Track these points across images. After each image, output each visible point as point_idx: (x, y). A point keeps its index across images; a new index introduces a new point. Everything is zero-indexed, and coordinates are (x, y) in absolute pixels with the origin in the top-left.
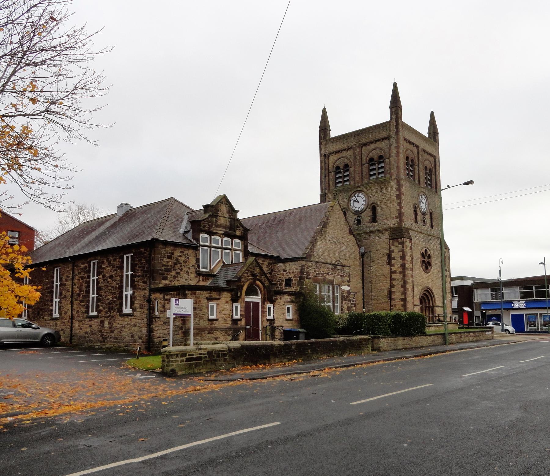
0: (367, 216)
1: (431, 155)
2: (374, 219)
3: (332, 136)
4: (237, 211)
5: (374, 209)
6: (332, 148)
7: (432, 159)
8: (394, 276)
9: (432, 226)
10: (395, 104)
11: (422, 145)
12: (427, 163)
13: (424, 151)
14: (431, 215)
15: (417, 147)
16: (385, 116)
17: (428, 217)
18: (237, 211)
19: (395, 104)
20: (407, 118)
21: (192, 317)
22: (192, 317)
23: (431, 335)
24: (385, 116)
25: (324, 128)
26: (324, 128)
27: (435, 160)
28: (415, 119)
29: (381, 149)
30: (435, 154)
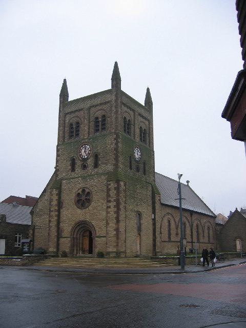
0: (90, 162)
1: (146, 119)
2: (96, 165)
3: (70, 99)
4: (236, 210)
5: (96, 157)
7: (147, 123)
8: (109, 210)
10: (116, 78)
11: (142, 112)
12: (142, 124)
15: (133, 111)
16: (108, 86)
17: (141, 166)
18: (236, 210)
19: (116, 78)
20: (125, 88)
23: (65, 237)
24: (108, 86)
25: (64, 93)
26: (64, 93)
27: (150, 121)
28: (134, 89)
29: (103, 110)
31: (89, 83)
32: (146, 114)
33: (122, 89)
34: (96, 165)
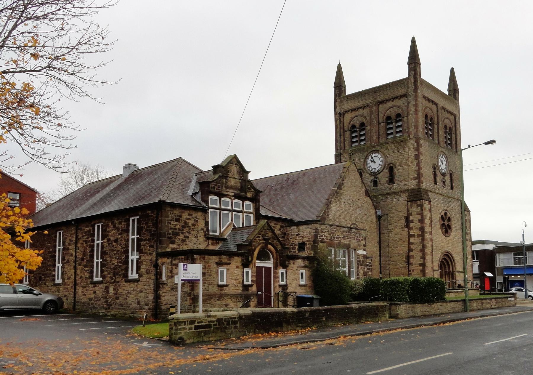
0: (384, 177)
2: (391, 180)
3: (347, 94)
5: (391, 170)
6: (348, 106)
7: (452, 117)
9: (452, 188)
11: (442, 103)
12: (447, 121)
13: (444, 109)
14: (451, 176)
15: (436, 105)
16: (403, 73)
17: (447, 178)
18: (248, 172)
20: (426, 74)
21: (201, 282)
22: (201, 282)
23: (451, 302)
24: (403, 73)
25: (339, 85)
26: (339, 85)
27: (455, 118)
29: (399, 107)
30: (455, 112)
31: (378, 69)
32: (449, 107)
33: (423, 76)
34: (391, 180)
